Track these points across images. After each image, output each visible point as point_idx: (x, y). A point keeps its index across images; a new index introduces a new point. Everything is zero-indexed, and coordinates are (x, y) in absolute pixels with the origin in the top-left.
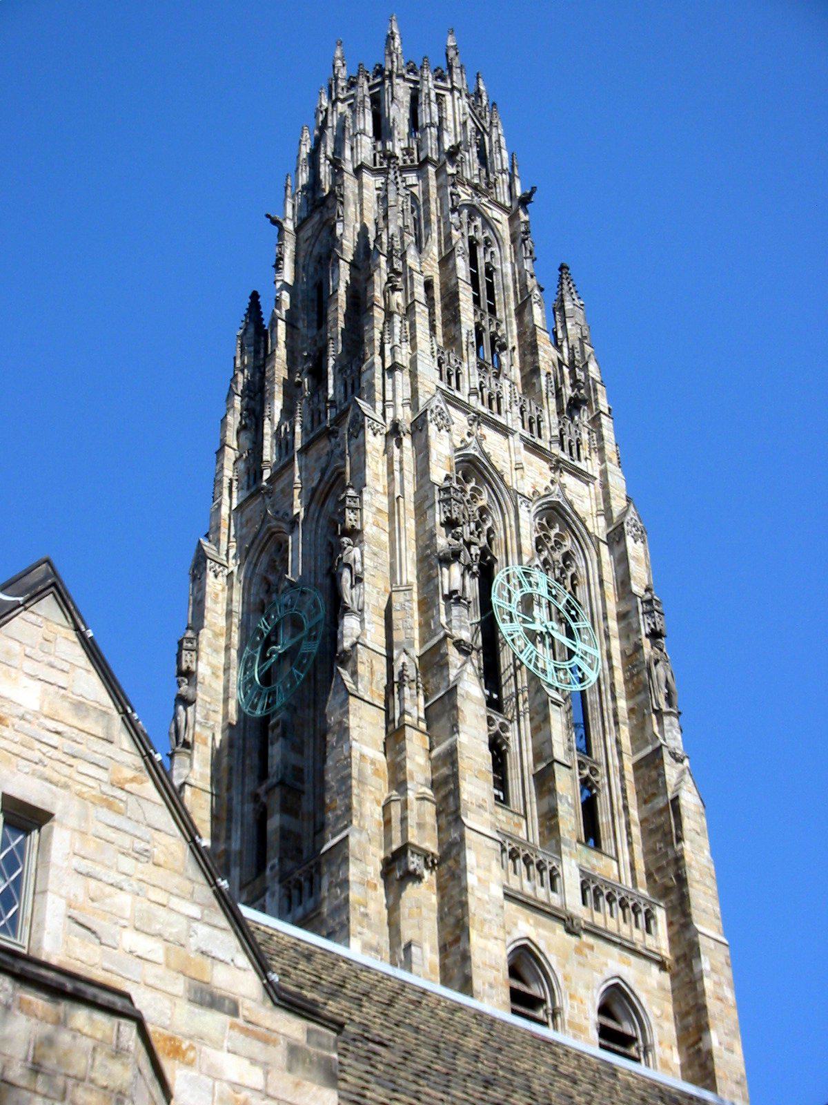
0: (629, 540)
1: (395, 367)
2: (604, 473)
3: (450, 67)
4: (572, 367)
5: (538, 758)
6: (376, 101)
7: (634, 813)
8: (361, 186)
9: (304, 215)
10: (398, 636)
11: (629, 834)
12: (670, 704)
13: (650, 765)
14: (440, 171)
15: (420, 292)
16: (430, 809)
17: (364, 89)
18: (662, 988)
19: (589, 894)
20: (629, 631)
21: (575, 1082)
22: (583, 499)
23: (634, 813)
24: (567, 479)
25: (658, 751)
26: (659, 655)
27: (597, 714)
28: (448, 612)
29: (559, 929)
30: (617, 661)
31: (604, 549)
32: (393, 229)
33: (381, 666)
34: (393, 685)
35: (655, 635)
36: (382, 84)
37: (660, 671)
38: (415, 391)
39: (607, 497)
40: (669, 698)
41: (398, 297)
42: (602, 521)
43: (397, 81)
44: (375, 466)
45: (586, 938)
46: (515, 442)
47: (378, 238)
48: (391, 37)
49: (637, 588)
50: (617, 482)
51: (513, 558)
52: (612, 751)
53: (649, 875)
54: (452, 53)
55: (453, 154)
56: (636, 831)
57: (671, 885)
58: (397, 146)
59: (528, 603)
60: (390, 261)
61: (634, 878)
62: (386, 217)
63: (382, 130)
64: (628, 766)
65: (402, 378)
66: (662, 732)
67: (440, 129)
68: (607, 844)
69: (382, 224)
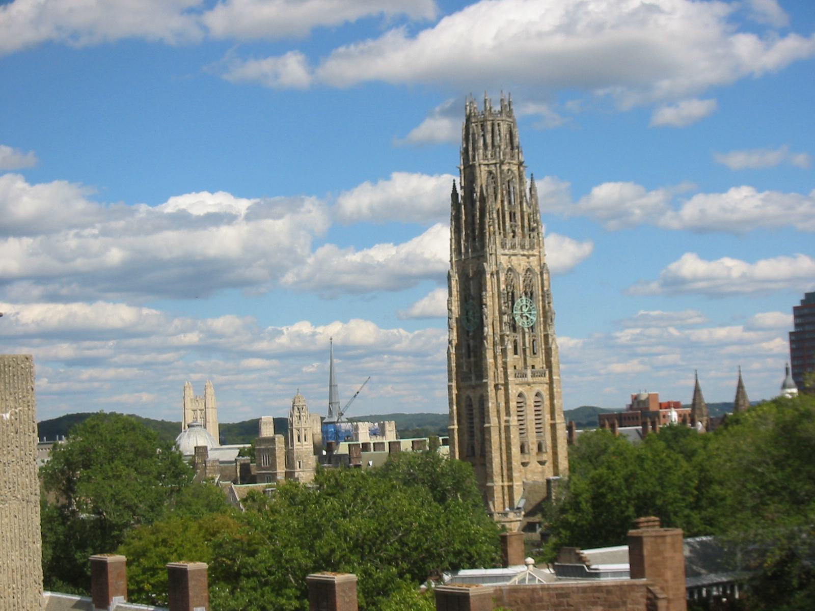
10: (495, 332)
15: (495, 215)
16: (502, 373)
18: (547, 388)
21: (521, 307)
33: (492, 338)
34: (494, 345)
44: (489, 284)
64: (542, 335)
65: (493, 256)
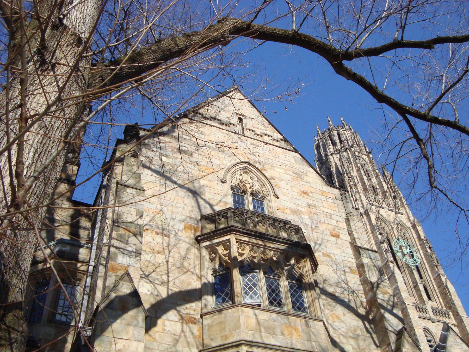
0: (417, 227)
1: (356, 200)
2: (406, 212)
3: (344, 125)
4: (391, 188)
5: (413, 283)
6: (330, 136)
7: (437, 290)
8: (333, 158)
9: (320, 166)
11: (437, 296)
12: (438, 263)
13: (438, 277)
14: (350, 150)
17: (327, 135)
19: (434, 312)
20: (424, 248)
22: (403, 219)
23: (437, 290)
24: (399, 215)
25: (439, 275)
26: (433, 253)
27: (421, 269)
28: (386, 254)
29: (430, 322)
30: (423, 256)
31: (412, 230)
32: (346, 167)
35: (430, 248)
36: (330, 132)
37: (434, 256)
38: (362, 204)
39: (409, 217)
40: (437, 262)
41: (351, 183)
42: (409, 223)
43: (333, 131)
45: (437, 323)
46: (386, 210)
47: (343, 170)
48: (329, 121)
49: (423, 238)
50: (410, 214)
51: (394, 238)
52: (428, 277)
53: (445, 305)
54: (343, 122)
55: (352, 146)
56: (439, 295)
57: (450, 305)
58: (339, 147)
59: (400, 247)
60: (347, 175)
61: (442, 306)
62: (343, 165)
63: (334, 144)
66: (438, 270)
67: (347, 141)
68: (432, 298)
69: (342, 167)
